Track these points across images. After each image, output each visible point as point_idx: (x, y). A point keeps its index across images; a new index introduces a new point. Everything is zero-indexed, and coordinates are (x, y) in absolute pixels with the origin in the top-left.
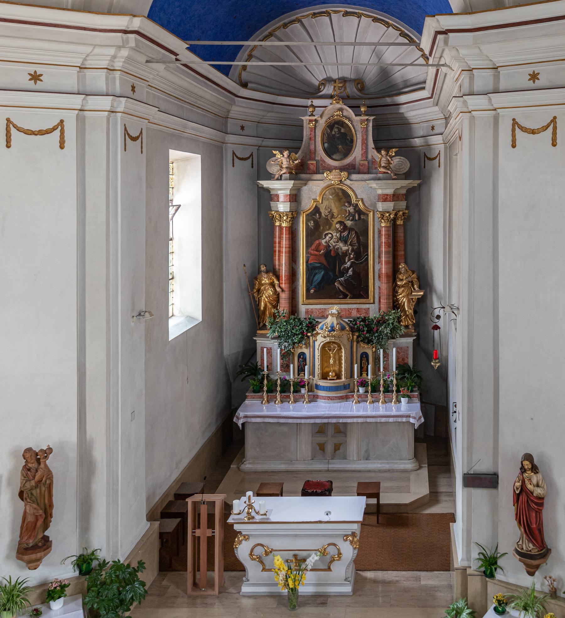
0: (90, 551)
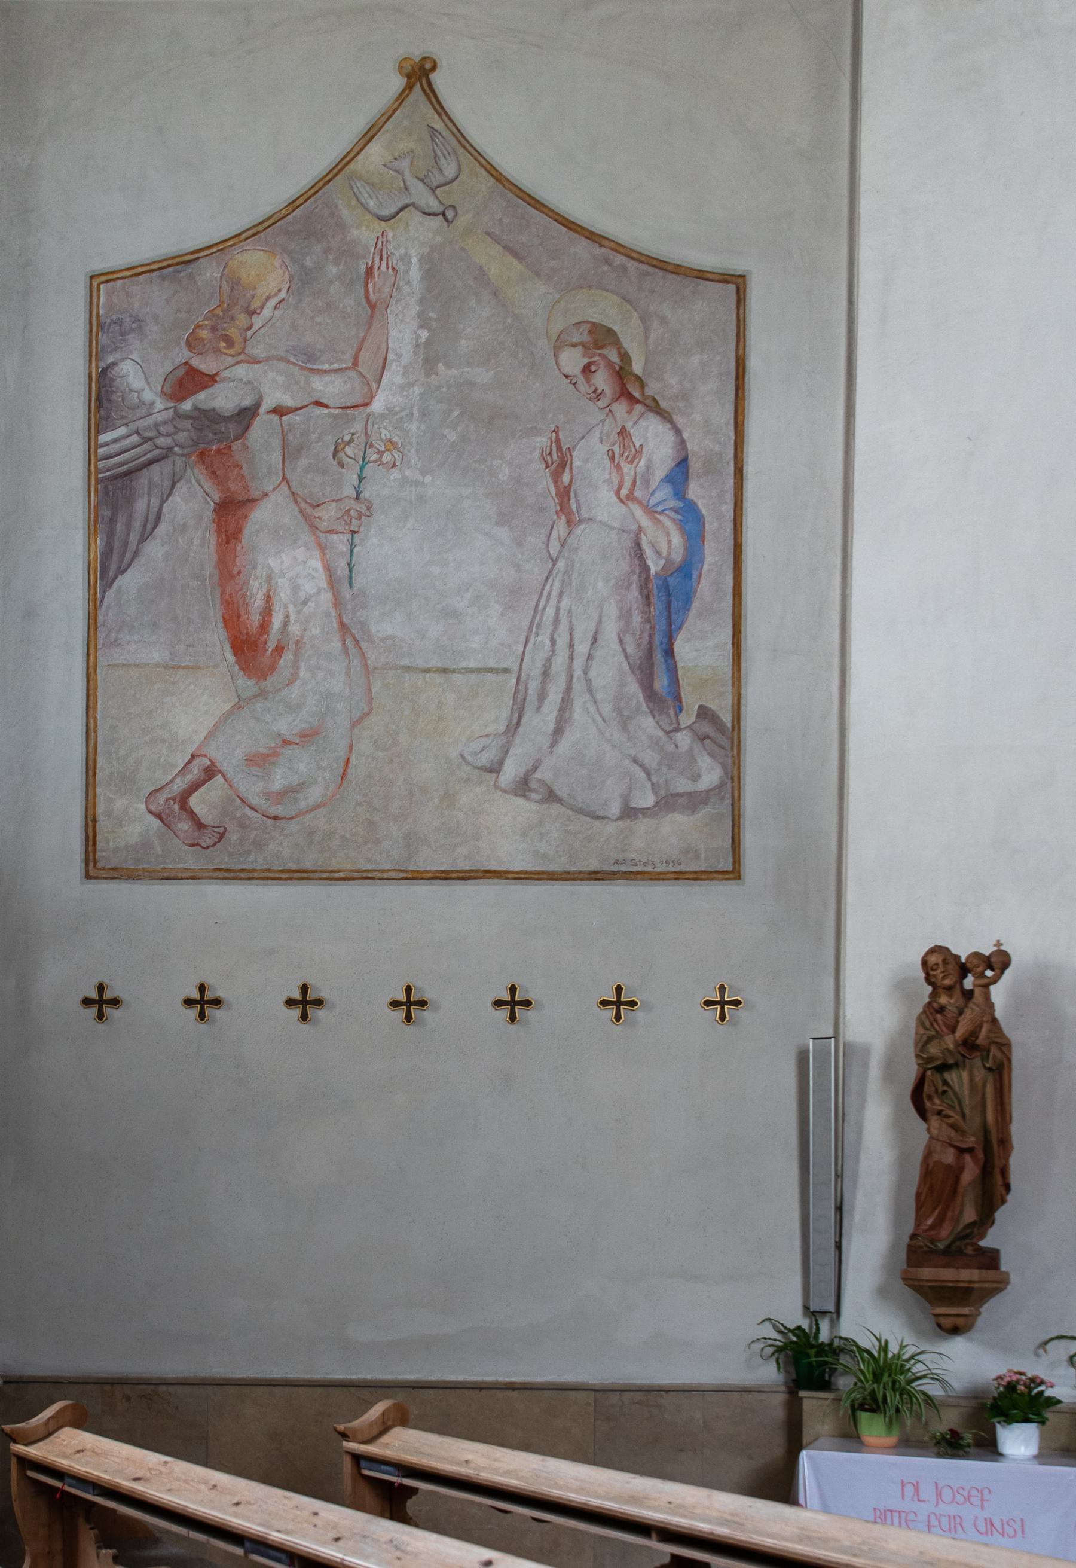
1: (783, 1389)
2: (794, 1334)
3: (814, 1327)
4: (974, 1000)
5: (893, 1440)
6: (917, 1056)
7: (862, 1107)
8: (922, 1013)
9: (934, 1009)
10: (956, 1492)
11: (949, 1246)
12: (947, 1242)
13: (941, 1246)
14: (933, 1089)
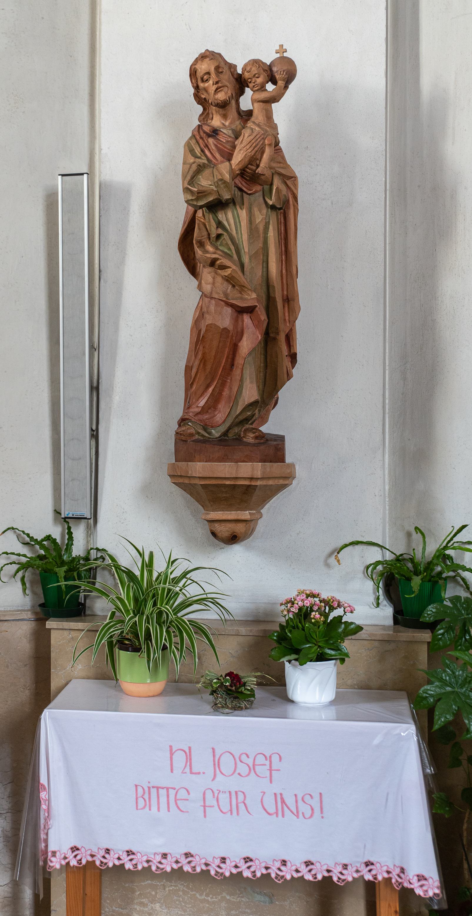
0: (432, 548)
1: (29, 615)
2: (42, 547)
3: (67, 537)
4: (253, 119)
5: (159, 685)
6: (186, 190)
7: (121, 262)
8: (191, 138)
9: (205, 132)
10: (237, 760)
11: (225, 433)
12: (223, 429)
13: (216, 433)
14: (205, 233)
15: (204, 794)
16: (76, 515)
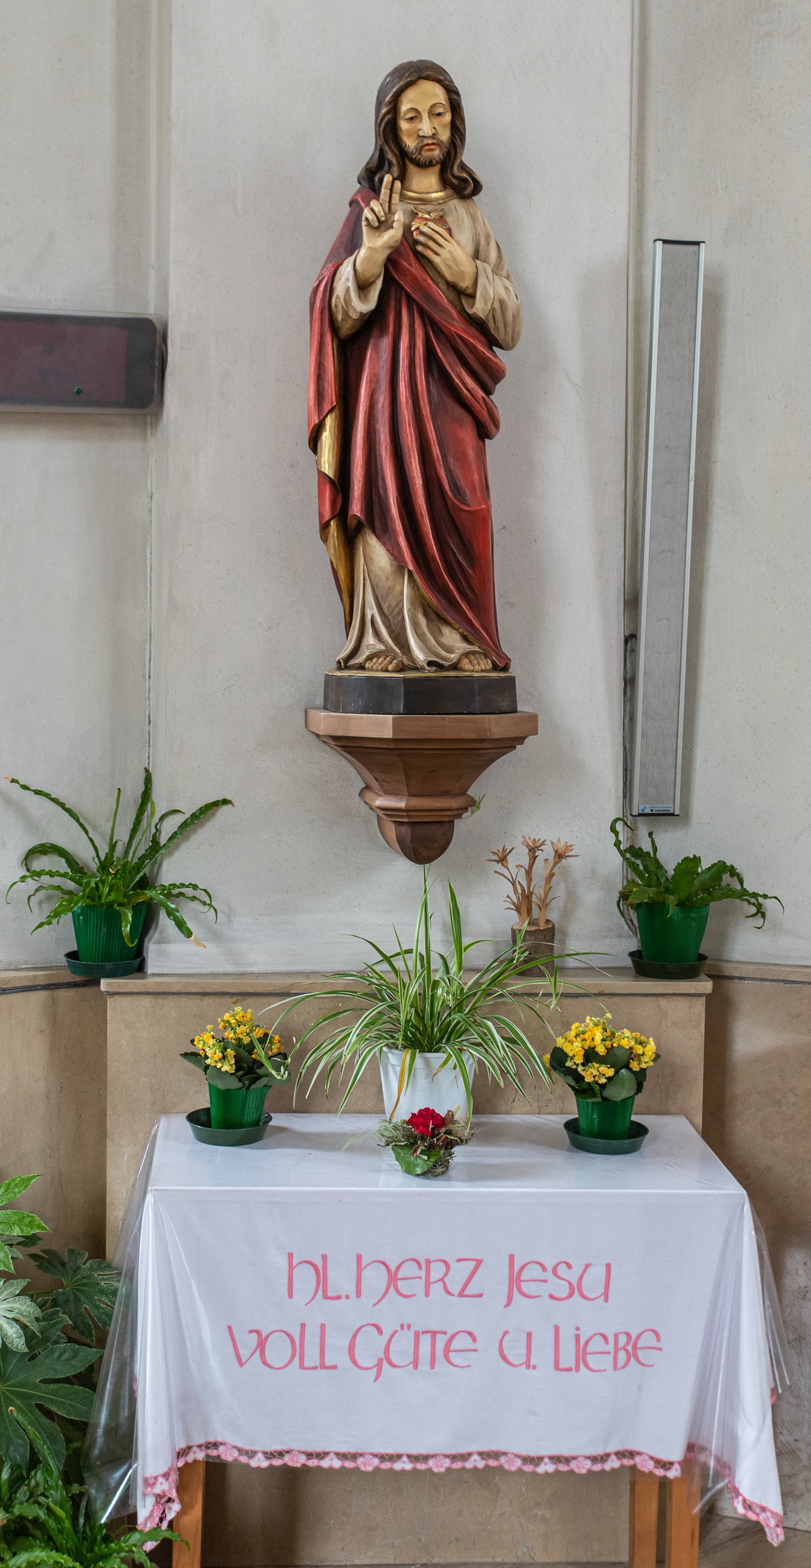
15: (210, 897)
16: (656, 811)
